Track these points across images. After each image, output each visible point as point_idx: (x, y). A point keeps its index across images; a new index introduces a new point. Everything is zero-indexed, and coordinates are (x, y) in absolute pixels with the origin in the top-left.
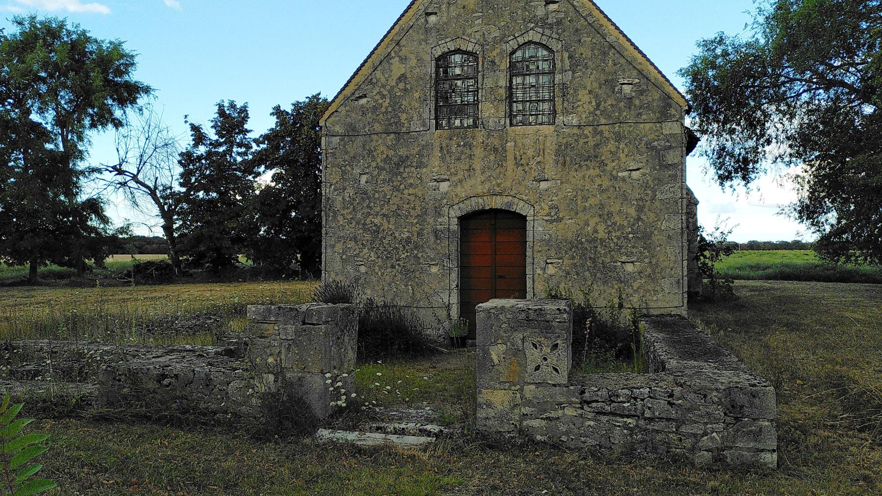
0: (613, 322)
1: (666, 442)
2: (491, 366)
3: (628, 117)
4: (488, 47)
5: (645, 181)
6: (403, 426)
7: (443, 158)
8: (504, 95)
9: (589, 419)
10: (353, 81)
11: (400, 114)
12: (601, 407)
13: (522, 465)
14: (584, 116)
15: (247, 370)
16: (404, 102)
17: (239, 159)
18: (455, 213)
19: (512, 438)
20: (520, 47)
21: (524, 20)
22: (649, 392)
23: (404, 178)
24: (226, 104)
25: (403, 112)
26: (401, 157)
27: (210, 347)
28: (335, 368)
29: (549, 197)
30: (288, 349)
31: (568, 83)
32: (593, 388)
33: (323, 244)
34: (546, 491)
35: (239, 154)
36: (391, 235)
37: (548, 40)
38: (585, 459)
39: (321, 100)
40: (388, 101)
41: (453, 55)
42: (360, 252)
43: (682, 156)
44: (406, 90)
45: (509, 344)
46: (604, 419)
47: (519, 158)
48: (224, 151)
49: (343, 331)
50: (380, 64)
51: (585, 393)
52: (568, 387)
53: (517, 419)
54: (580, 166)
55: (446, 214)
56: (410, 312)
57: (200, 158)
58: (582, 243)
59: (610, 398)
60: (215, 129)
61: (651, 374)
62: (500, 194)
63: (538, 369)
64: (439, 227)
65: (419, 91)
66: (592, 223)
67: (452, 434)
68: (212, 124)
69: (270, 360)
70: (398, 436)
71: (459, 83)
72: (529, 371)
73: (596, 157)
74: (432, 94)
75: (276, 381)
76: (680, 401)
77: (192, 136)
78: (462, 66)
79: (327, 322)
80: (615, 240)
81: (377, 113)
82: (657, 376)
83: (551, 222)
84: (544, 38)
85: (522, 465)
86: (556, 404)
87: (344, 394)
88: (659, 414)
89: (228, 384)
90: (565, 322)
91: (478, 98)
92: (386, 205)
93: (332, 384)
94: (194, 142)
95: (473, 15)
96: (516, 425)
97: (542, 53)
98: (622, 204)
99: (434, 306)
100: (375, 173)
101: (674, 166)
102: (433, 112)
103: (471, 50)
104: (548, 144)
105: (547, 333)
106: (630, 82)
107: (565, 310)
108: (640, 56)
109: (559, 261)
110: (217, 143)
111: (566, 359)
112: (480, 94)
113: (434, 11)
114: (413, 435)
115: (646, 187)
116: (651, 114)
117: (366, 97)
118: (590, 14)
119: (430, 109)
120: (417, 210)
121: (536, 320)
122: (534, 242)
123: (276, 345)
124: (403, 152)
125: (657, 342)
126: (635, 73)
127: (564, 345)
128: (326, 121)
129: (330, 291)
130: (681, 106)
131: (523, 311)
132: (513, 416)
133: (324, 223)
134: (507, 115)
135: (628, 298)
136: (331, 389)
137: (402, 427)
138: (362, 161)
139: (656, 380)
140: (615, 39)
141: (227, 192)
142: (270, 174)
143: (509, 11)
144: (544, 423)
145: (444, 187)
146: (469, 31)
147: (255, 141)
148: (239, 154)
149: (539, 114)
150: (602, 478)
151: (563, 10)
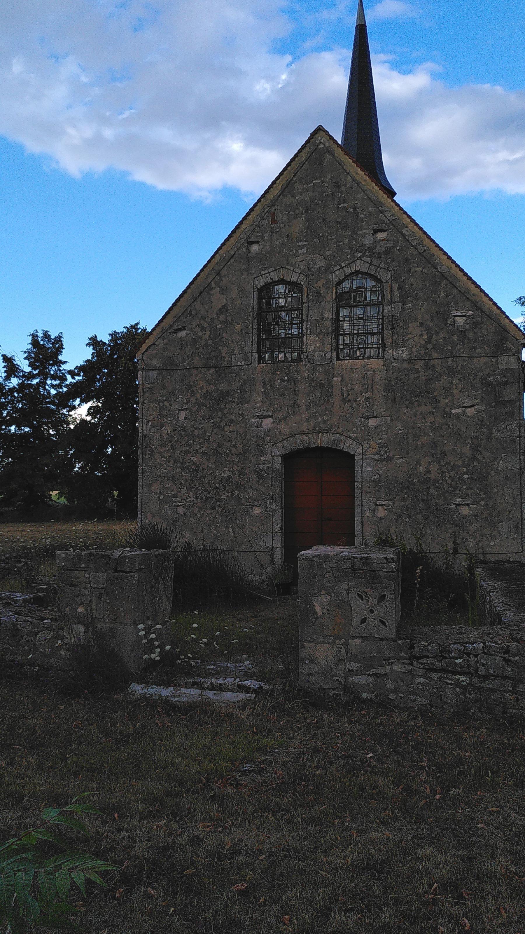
0: (447, 568)
1: (501, 701)
2: (314, 618)
3: (462, 351)
4: (313, 277)
5: (480, 418)
6: (220, 681)
7: (266, 394)
8: (330, 328)
9: (419, 676)
10: (171, 312)
11: (220, 348)
12: (432, 663)
13: (347, 725)
14: (414, 350)
15: (55, 620)
16: (224, 335)
17: (53, 392)
18: (278, 451)
19: (337, 695)
20: (346, 277)
21: (351, 248)
22: (483, 647)
23: (225, 414)
24: (40, 334)
25: (225, 345)
26: (221, 392)
27: (18, 595)
28: (148, 618)
29: (378, 435)
30: (99, 598)
31: (398, 315)
32: (422, 643)
33: (140, 483)
34: (371, 755)
35: (53, 386)
36: (211, 474)
37: (376, 270)
38: (415, 719)
39: (140, 330)
40: (208, 333)
41: (276, 285)
42: (178, 492)
43: (520, 393)
44: (226, 322)
45: (333, 594)
46: (435, 676)
47: (346, 393)
48: (37, 383)
49: (158, 579)
50: (200, 294)
51: (414, 648)
52: (396, 641)
53: (342, 675)
54: (411, 403)
55: (269, 452)
56: (230, 556)
57: (12, 390)
58: (414, 484)
59: (441, 653)
60: (28, 360)
61: (485, 628)
62: (327, 432)
63: (365, 622)
64: (261, 466)
65: (241, 323)
66: (425, 462)
67: (272, 691)
68: (25, 355)
69: (81, 610)
70: (215, 692)
71: (283, 314)
72: (354, 624)
73: (428, 393)
74: (254, 327)
75: (87, 632)
76: (517, 658)
77: (4, 367)
78: (286, 297)
79: (139, 570)
80: (449, 481)
81: (197, 346)
82: (493, 629)
83: (382, 461)
84: (372, 268)
85: (347, 725)
86: (384, 660)
87: (159, 647)
88: (494, 672)
89: (36, 635)
90: (393, 572)
91: (302, 331)
92: (206, 443)
93: (145, 637)
94: (6, 374)
95: (298, 244)
96: (340, 682)
97: (369, 283)
98: (456, 442)
99: (256, 550)
100: (194, 409)
101: (511, 402)
102: (255, 345)
103: (295, 280)
104: (377, 379)
105: (374, 583)
106: (463, 314)
107: (392, 558)
108: (473, 286)
109: (390, 502)
110: (30, 375)
111: (394, 611)
112: (305, 327)
113: (256, 240)
114: (232, 691)
115: (482, 425)
116: (486, 348)
117: (185, 329)
118: (420, 243)
119: (252, 342)
120: (238, 449)
121: (362, 570)
122: (362, 482)
123: (87, 593)
124: (223, 387)
125: (493, 592)
126: (468, 304)
127: (391, 596)
128: (143, 354)
129: (146, 533)
130: (517, 340)
131: (347, 559)
132: (338, 673)
133: (140, 461)
134: (333, 349)
135: (464, 543)
136: (145, 641)
137: (219, 682)
138: (180, 397)
139: (490, 634)
140: (448, 270)
141: (40, 426)
142: (86, 407)
143: (335, 240)
144: (371, 679)
145: (267, 423)
146: (293, 261)
147: (72, 373)
148: (53, 386)
149: (368, 348)
150: (432, 741)
151: (392, 238)
